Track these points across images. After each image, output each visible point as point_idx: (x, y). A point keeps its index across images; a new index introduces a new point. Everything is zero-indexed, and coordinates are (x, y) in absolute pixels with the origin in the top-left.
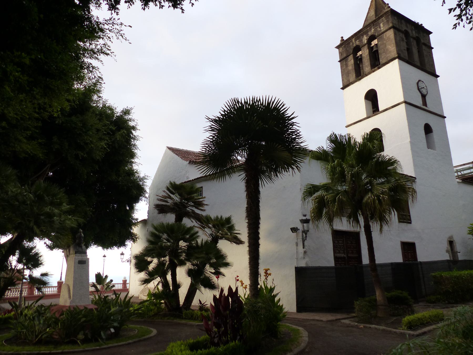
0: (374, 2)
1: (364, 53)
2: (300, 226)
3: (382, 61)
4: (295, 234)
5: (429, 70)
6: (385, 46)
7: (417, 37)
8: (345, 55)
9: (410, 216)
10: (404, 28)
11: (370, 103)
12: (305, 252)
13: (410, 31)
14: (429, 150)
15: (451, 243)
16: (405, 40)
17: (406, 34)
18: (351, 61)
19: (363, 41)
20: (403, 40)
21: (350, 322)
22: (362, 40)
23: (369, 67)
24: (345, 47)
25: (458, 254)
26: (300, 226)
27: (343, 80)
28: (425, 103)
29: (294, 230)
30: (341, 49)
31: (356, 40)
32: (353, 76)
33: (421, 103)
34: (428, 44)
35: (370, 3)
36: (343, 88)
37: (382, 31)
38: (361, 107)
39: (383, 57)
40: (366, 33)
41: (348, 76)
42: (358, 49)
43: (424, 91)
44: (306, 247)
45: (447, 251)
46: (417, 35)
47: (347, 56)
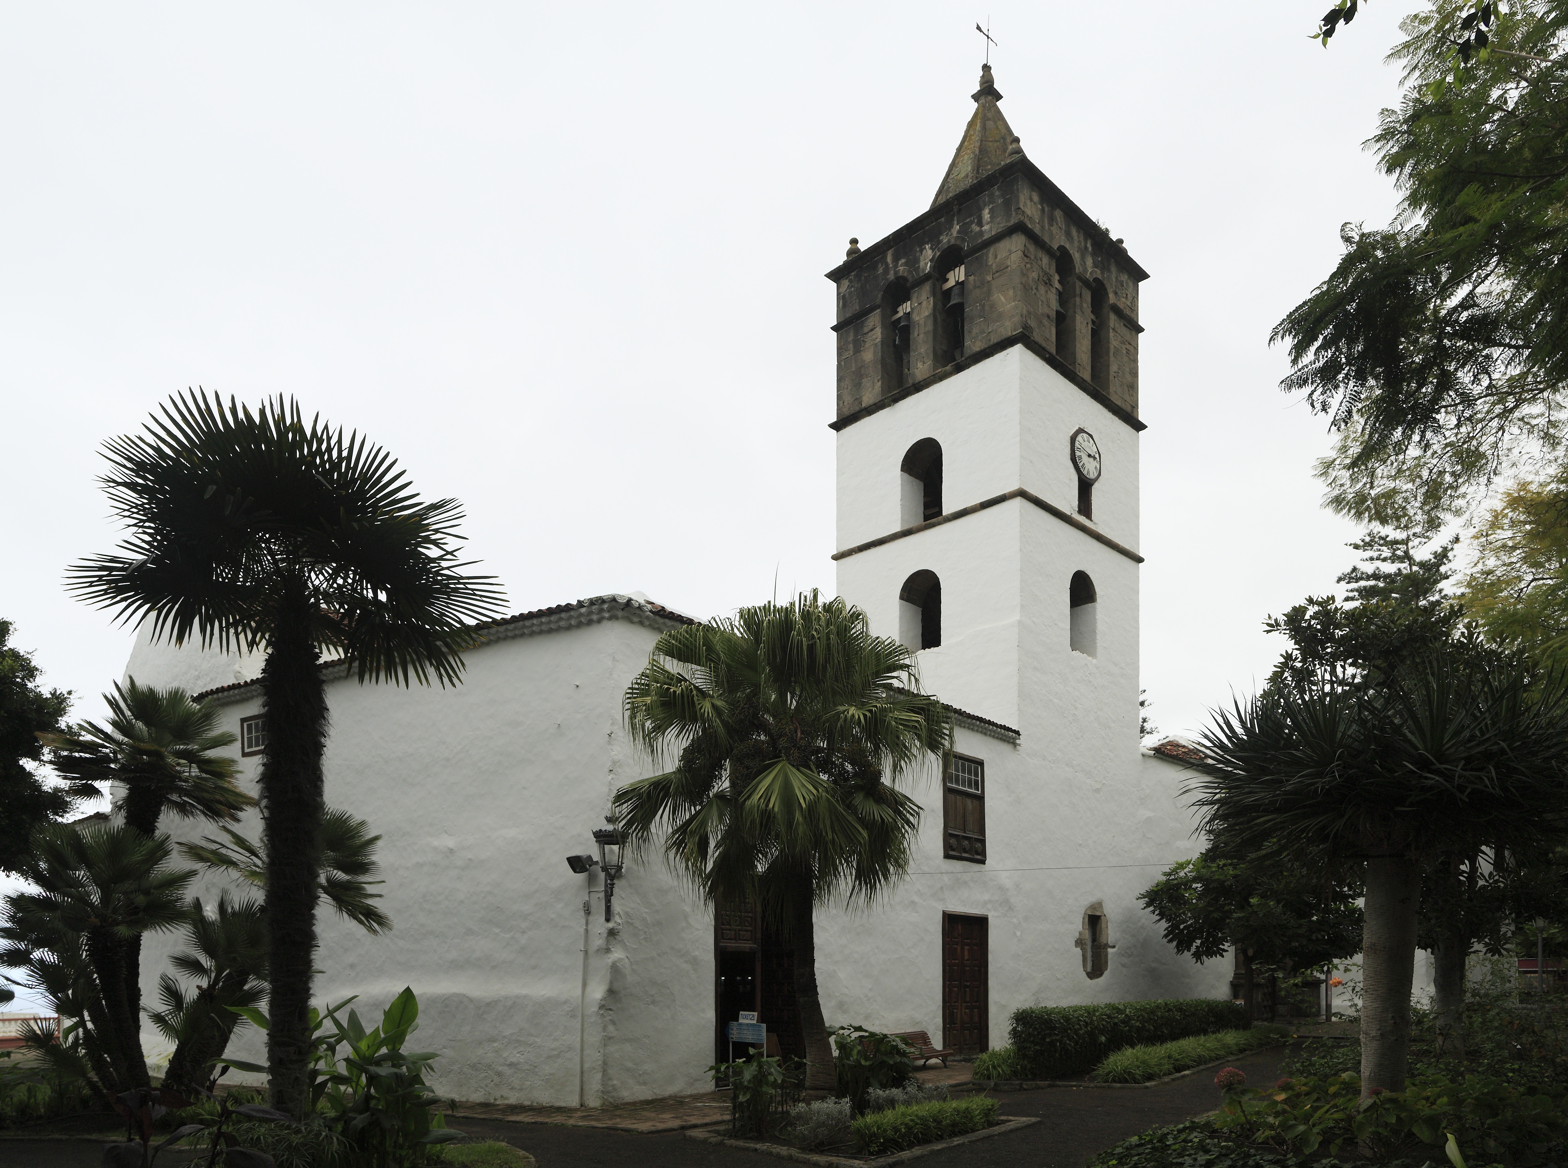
0: (978, 127)
1: (919, 308)
2: (592, 850)
3: (973, 345)
4: (581, 877)
5: (1119, 403)
6: (989, 293)
7: (1096, 280)
8: (856, 307)
9: (983, 842)
10: (1057, 238)
11: (917, 487)
12: (612, 933)
13: (1076, 256)
14: (1076, 653)
15: (1094, 921)
16: (1057, 285)
17: (1063, 261)
18: (875, 331)
19: (922, 264)
20: (1048, 283)
21: (707, 1135)
22: (917, 261)
23: (929, 363)
25: (1110, 950)
26: (592, 850)
27: (839, 397)
28: (1085, 507)
29: (577, 864)
30: (846, 283)
31: (896, 260)
33: (1075, 503)
34: (1127, 312)
35: (965, 128)
36: (837, 426)
37: (986, 237)
38: (890, 499)
39: (975, 331)
40: (933, 238)
41: (858, 385)
42: (900, 291)
43: (1090, 467)
45: (1079, 943)
46: (1098, 274)
47: (864, 314)
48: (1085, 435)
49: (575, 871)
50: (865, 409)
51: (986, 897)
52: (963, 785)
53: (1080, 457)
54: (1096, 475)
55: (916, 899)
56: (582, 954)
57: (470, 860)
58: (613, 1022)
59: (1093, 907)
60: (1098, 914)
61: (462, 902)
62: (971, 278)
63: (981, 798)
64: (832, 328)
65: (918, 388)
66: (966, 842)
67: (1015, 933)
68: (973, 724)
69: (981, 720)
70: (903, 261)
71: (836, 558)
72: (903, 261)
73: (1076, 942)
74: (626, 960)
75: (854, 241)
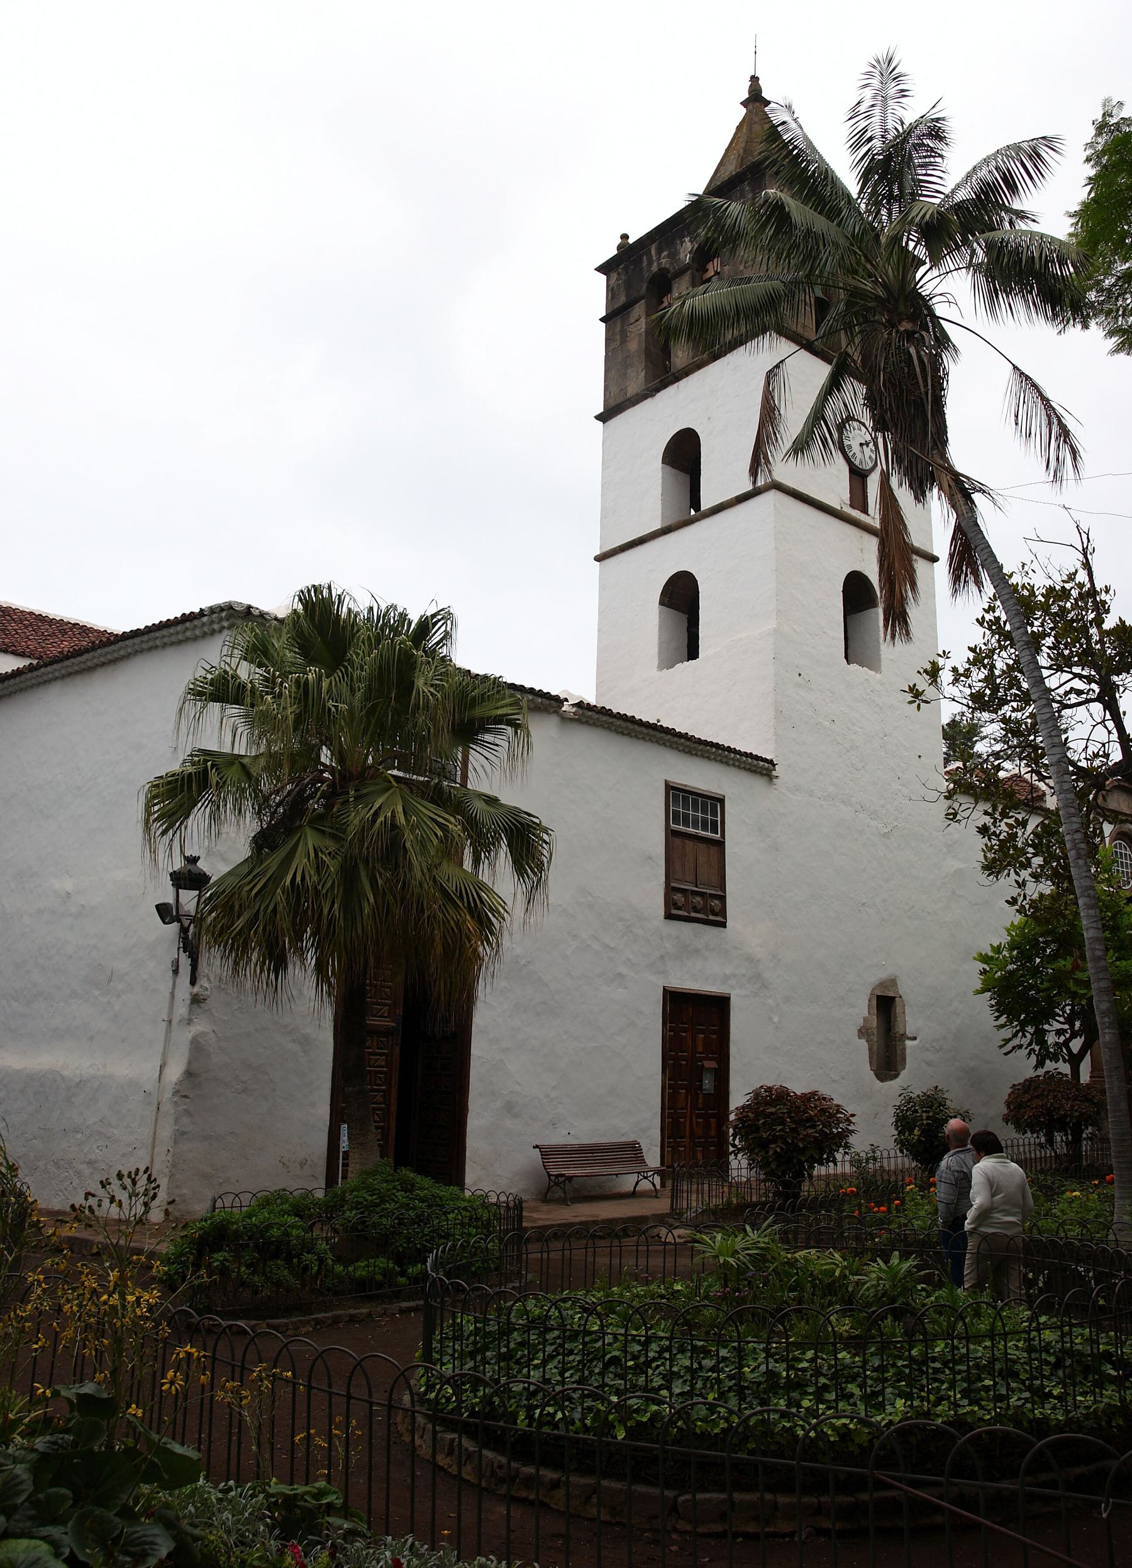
8: (622, 299)
9: (723, 899)
11: (686, 479)
14: (854, 667)
15: (886, 1005)
18: (639, 322)
19: (682, 256)
24: (626, 269)
25: (908, 1043)
30: (614, 276)
31: (659, 252)
32: (636, 381)
33: (846, 496)
36: (603, 418)
38: (650, 492)
44: (203, 982)
45: (863, 1032)
48: (855, 424)
49: (164, 923)
50: (629, 399)
51: (728, 970)
52: (695, 826)
53: (850, 446)
54: (871, 465)
55: (624, 970)
56: (164, 1024)
57: (83, 906)
58: (188, 1113)
59: (882, 984)
60: (891, 994)
61: (71, 957)
62: (726, 268)
63: (720, 844)
64: (601, 320)
65: (677, 377)
66: (698, 899)
67: (770, 1019)
68: (707, 751)
69: (717, 746)
70: (665, 253)
71: (599, 559)
72: (665, 253)
73: (860, 1031)
74: (212, 1035)
75: (625, 237)
